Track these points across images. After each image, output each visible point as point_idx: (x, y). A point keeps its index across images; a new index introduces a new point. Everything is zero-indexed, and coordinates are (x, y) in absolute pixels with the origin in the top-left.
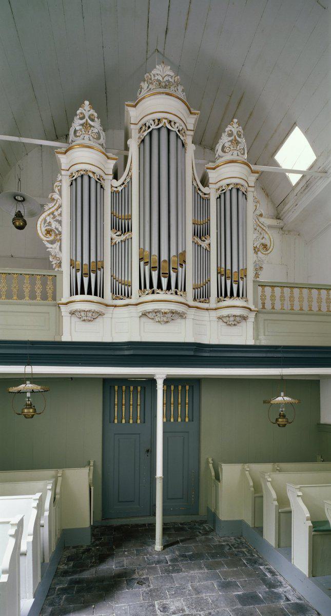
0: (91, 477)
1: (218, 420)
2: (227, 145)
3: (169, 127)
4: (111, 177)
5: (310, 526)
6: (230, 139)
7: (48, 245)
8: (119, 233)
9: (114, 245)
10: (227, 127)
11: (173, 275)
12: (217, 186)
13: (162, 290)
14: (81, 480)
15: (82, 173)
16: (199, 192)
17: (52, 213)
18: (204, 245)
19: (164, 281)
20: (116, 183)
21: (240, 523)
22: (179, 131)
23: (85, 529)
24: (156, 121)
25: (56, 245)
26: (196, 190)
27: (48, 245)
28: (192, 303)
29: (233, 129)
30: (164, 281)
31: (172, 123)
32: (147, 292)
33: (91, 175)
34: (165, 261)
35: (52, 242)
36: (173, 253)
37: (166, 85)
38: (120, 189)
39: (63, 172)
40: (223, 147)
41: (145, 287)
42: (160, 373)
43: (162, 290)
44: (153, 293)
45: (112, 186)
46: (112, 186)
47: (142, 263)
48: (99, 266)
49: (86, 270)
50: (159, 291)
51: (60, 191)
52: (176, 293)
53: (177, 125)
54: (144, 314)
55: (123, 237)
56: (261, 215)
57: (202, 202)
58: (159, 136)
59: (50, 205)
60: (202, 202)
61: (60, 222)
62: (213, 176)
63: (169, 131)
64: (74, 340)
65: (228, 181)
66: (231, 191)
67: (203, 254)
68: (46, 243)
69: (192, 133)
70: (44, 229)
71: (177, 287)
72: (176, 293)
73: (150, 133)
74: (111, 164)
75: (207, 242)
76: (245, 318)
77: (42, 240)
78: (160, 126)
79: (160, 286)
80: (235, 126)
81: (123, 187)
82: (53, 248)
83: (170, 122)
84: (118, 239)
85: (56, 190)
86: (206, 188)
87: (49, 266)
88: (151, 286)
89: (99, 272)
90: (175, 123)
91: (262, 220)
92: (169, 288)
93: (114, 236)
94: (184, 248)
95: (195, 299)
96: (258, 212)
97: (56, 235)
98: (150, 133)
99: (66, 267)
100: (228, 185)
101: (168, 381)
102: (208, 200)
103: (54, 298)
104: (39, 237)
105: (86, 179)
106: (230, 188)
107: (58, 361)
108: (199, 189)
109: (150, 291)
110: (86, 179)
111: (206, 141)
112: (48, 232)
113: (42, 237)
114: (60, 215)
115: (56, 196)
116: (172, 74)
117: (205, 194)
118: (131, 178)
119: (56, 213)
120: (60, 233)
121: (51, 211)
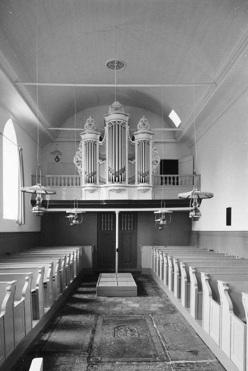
0: (93, 251)
1: (142, 233)
2: (141, 125)
3: (118, 124)
4: (99, 140)
5: (185, 281)
6: (142, 123)
7: (77, 166)
8: (102, 160)
9: (100, 165)
10: (141, 119)
11: (120, 176)
12: (108, 122)
13: (116, 182)
14: (89, 250)
15: (89, 141)
16: (131, 143)
17: (79, 155)
18: (133, 163)
19: (117, 179)
20: (100, 142)
21: (150, 269)
22: (122, 124)
23: (91, 268)
24: (114, 122)
25: (80, 166)
26: (129, 142)
27: (77, 166)
28: (127, 185)
29: (143, 120)
30: (117, 179)
31: (120, 122)
32: (111, 183)
33: (92, 142)
34: (117, 172)
35: (79, 165)
36: (120, 169)
37: (117, 109)
38: (102, 144)
39: (82, 140)
40: (140, 126)
41: (111, 181)
42: (117, 211)
43: (116, 182)
44: (113, 183)
45: (99, 144)
46: (99, 144)
47: (110, 172)
48: (95, 173)
49: (90, 175)
50: (115, 182)
51: (81, 147)
52: (121, 183)
53: (121, 122)
54: (111, 190)
55: (103, 162)
56: (155, 149)
57: (132, 147)
58: (117, 127)
59: (78, 152)
60: (132, 147)
61: (81, 158)
62: (136, 137)
63: (118, 125)
64: (87, 200)
65: (142, 139)
66: (142, 143)
67: (132, 167)
68: (76, 165)
69: (128, 122)
70: (76, 161)
71: (121, 181)
72: (121, 183)
73: (112, 126)
74: (99, 136)
75: (134, 161)
76: (148, 190)
77: (75, 165)
78: (115, 124)
79: (115, 181)
80: (144, 118)
81: (103, 144)
82: (79, 167)
83: (119, 122)
84: (101, 163)
85: (80, 146)
86: (134, 141)
87: (78, 174)
88: (112, 181)
89: (94, 175)
90: (121, 122)
91: (156, 151)
92: (119, 181)
93: (100, 162)
94: (124, 165)
95: (129, 184)
96: (154, 148)
97: (80, 162)
98: (112, 126)
99: (83, 174)
100: (141, 141)
101: (121, 213)
102: (135, 145)
103: (79, 185)
104: (74, 163)
105: (90, 143)
106: (142, 142)
107: (82, 204)
108: (131, 142)
109: (112, 182)
110: (90, 143)
111: (133, 124)
112: (77, 162)
113: (75, 163)
114: (81, 155)
115: (80, 149)
116: (120, 104)
117: (133, 143)
118: (106, 141)
119: (80, 155)
120: (81, 162)
121: (78, 154)
